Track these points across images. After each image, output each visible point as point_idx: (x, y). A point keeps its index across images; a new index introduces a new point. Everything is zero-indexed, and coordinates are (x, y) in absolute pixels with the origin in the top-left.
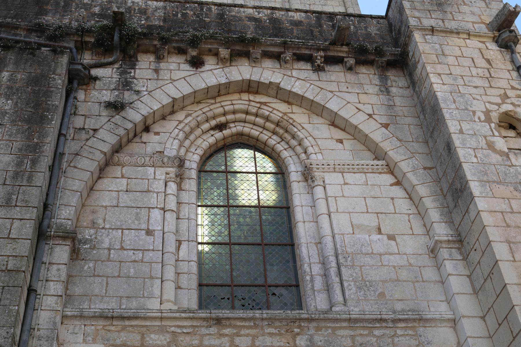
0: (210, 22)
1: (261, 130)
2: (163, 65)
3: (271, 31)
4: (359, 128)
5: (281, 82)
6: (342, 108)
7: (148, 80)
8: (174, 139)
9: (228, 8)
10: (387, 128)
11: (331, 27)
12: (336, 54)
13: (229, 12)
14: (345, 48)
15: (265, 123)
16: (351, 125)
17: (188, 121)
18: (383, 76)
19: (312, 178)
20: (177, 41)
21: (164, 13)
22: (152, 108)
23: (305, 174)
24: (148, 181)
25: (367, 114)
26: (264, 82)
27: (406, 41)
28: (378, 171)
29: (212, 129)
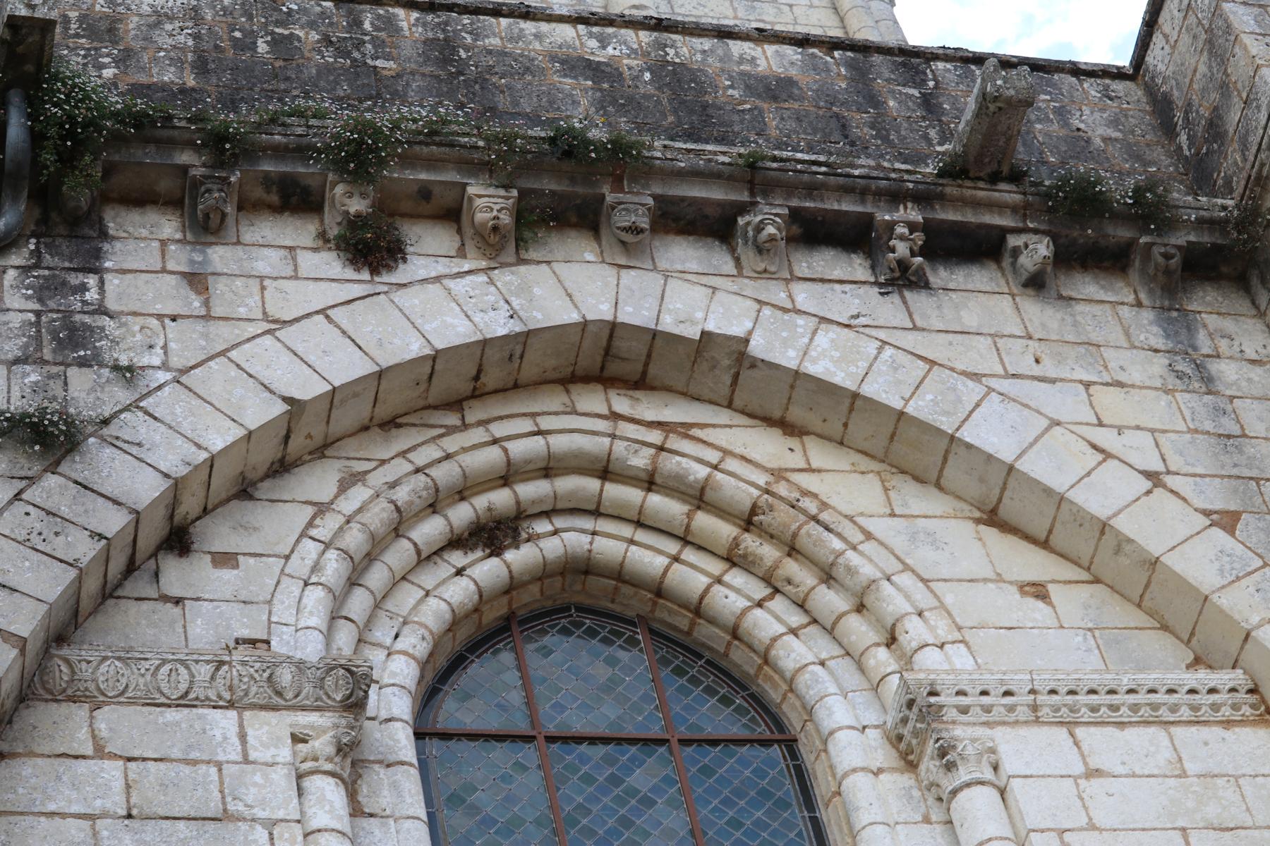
0: (399, 76)
1: (672, 547)
2: (219, 256)
3: (671, 119)
4: (1118, 533)
5: (750, 333)
6: (1031, 445)
7: (167, 321)
8: (306, 584)
9: (466, 20)
10: (1231, 530)
11: (919, 106)
12: (970, 217)
13: (476, 35)
14: (1008, 194)
15: (689, 516)
16: (1081, 517)
17: (356, 505)
18: (1175, 314)
19: (942, 753)
20: (279, 152)
21: (196, 37)
22: (200, 441)
23: (900, 738)
24: (220, 770)
25: (1141, 472)
26: (676, 331)
27: (1262, 165)
28: (1219, 716)
29: (456, 542)
